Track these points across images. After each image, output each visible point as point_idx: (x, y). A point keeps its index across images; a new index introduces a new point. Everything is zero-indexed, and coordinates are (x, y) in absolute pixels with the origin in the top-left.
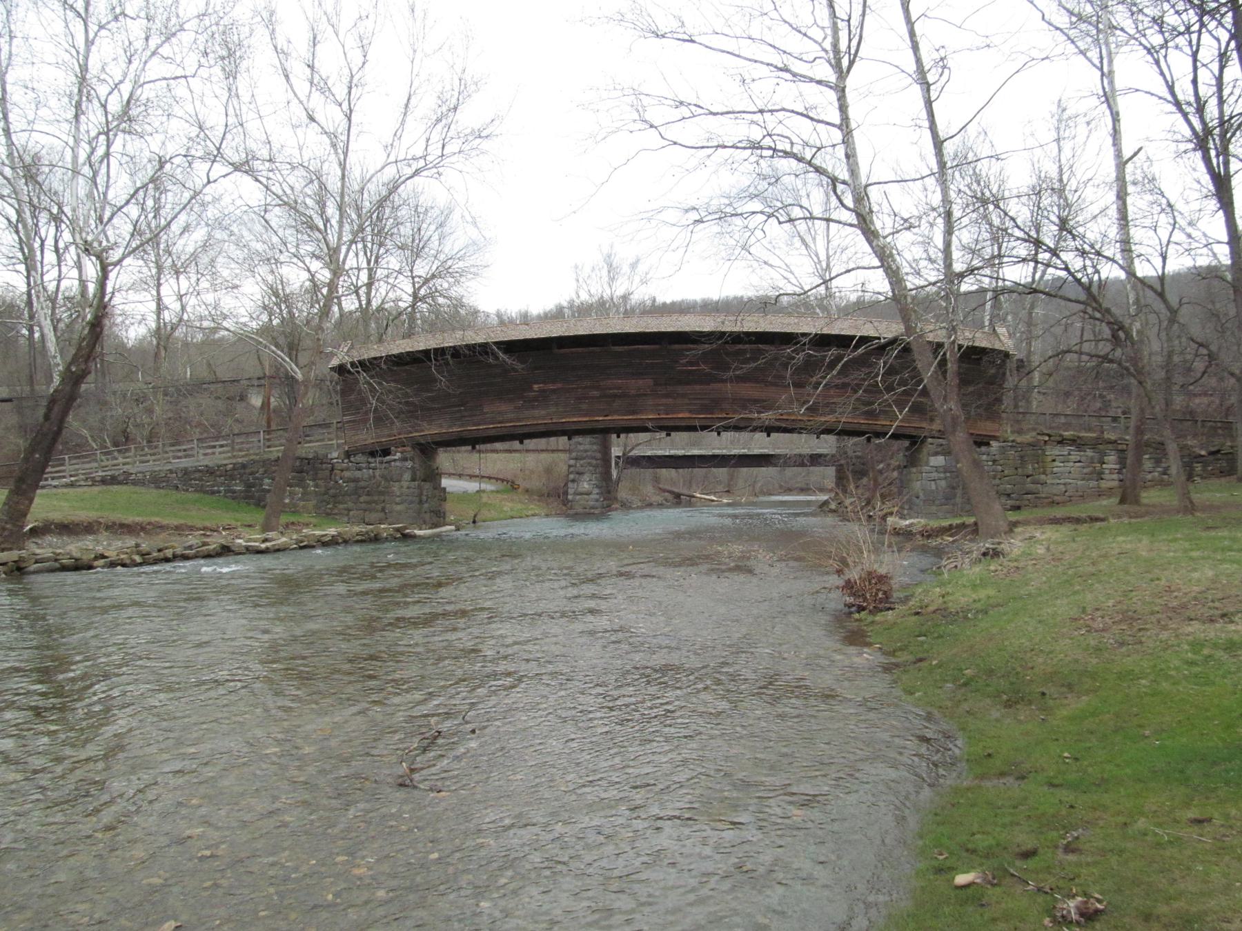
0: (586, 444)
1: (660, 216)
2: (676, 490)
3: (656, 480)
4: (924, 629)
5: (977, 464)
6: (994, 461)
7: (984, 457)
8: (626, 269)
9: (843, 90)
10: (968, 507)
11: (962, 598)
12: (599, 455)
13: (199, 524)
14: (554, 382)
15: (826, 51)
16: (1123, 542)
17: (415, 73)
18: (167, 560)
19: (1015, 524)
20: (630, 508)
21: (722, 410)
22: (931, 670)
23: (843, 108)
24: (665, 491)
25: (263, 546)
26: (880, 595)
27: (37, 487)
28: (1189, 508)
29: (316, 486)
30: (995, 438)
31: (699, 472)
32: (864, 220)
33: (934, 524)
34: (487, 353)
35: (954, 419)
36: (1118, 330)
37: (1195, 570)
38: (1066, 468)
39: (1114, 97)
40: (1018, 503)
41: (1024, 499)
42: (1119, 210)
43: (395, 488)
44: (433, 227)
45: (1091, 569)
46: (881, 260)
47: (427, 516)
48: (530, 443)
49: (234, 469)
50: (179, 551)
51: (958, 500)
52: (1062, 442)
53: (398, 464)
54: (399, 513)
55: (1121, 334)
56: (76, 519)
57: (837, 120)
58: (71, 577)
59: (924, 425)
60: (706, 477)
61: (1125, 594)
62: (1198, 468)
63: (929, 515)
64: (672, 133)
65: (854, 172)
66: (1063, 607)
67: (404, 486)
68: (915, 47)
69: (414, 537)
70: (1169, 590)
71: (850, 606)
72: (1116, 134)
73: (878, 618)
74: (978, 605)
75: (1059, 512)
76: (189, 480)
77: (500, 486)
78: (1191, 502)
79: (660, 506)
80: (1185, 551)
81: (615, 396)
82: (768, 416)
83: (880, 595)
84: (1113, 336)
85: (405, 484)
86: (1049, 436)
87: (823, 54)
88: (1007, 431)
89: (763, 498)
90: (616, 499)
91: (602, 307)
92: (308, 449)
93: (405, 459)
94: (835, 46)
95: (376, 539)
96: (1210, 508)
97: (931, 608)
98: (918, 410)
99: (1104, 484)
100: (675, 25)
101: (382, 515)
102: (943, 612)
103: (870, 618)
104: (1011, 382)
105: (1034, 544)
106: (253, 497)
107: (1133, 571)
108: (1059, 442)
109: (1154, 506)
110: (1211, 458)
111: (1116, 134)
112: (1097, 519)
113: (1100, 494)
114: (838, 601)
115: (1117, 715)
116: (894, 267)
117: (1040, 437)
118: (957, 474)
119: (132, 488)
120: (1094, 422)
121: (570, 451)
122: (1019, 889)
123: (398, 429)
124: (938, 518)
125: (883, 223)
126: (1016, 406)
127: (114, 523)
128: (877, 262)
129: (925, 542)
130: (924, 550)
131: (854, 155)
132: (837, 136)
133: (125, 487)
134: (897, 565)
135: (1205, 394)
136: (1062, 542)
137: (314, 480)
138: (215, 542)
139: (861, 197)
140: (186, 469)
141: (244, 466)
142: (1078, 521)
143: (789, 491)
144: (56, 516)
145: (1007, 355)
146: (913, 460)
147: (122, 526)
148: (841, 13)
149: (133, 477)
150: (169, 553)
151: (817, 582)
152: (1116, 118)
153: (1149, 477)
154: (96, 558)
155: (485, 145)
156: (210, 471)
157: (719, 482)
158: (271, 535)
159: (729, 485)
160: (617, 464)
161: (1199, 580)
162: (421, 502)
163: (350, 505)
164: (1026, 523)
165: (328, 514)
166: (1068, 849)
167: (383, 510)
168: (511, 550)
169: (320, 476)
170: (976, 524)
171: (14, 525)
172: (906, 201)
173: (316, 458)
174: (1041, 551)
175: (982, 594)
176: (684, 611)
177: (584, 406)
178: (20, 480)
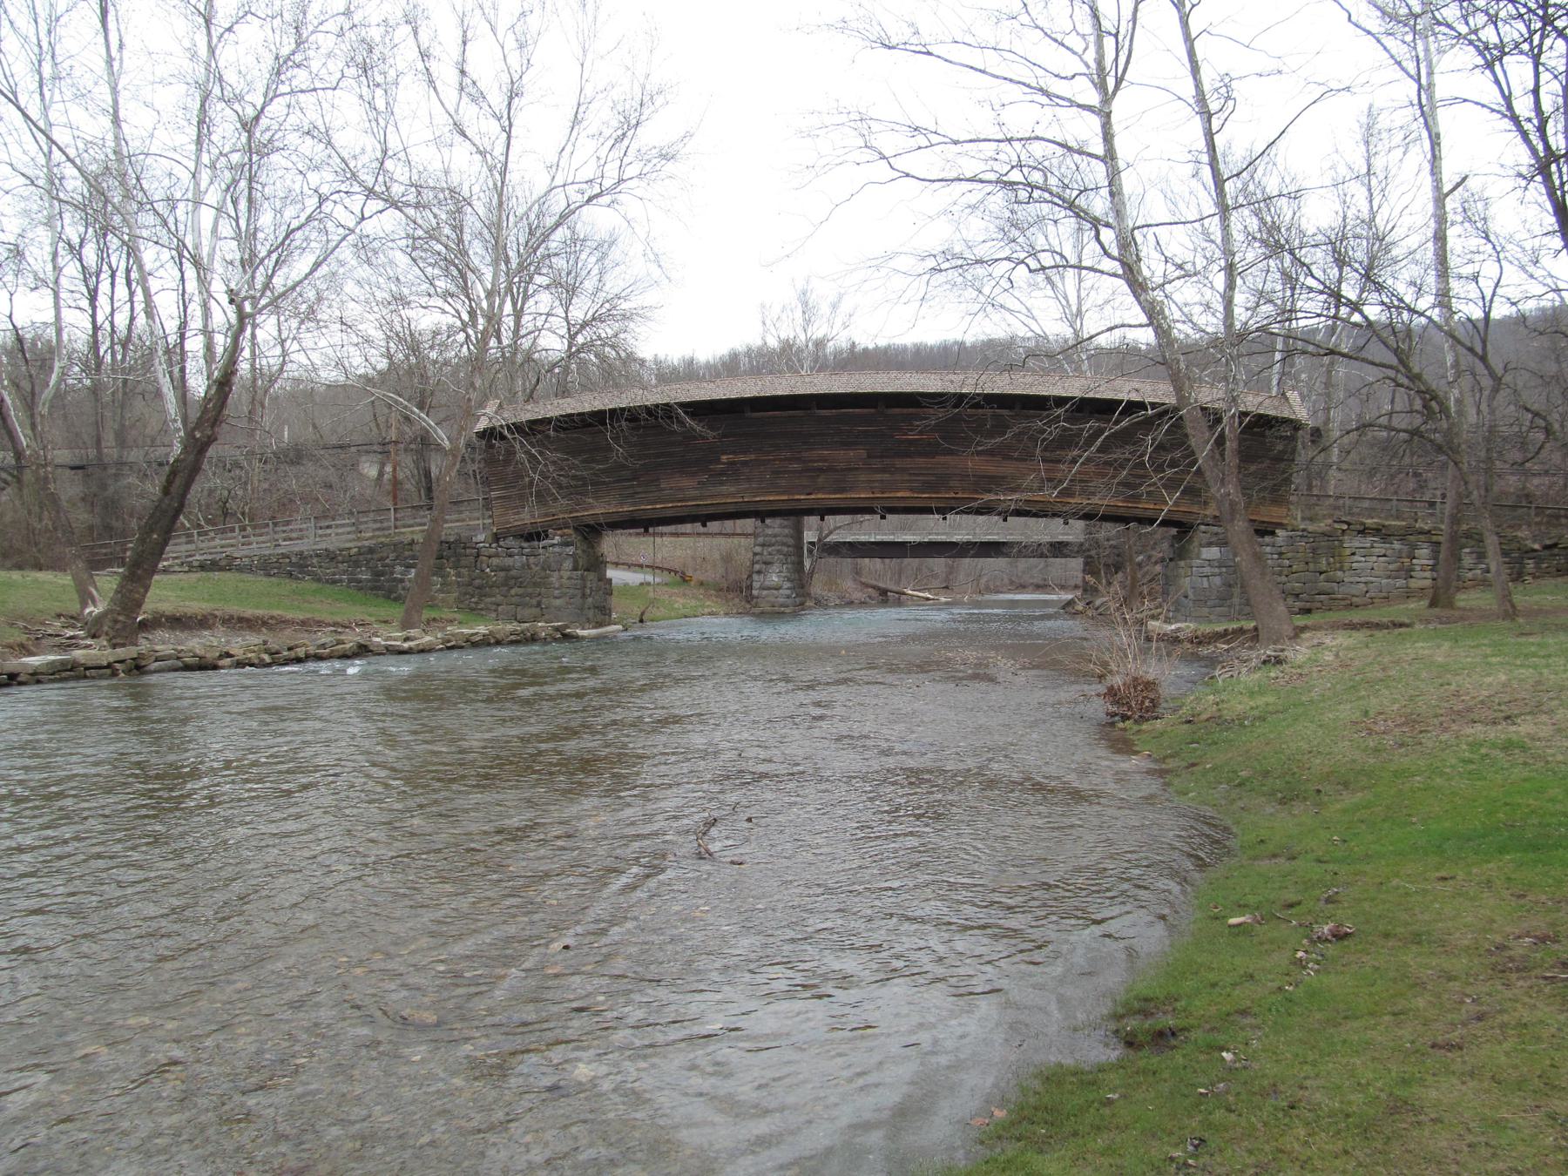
0: (775, 526)
1: (892, 264)
2: (881, 585)
3: (857, 572)
4: (1196, 737)
5: (1258, 558)
6: (1280, 554)
7: (1268, 549)
8: (825, 309)
9: (1108, 115)
10: (1247, 609)
11: (1238, 705)
12: (791, 541)
13: (329, 619)
14: (745, 453)
15: (1088, 67)
16: (1423, 648)
17: (585, 76)
18: (299, 660)
19: (1304, 629)
20: (826, 607)
21: (950, 489)
22: (1205, 772)
23: (1108, 137)
24: (867, 586)
25: (406, 645)
26: (1147, 703)
27: (154, 571)
28: (1511, 613)
29: (458, 575)
30: (1281, 526)
31: (911, 563)
32: (1131, 270)
33: (1207, 629)
34: (670, 418)
35: (1232, 504)
36: (1431, 401)
37: (1489, 675)
38: (1367, 564)
39: (1433, 108)
40: (1308, 605)
41: (1313, 602)
42: (1436, 254)
43: (554, 578)
44: (593, 259)
45: (1380, 675)
46: (1150, 317)
47: (591, 614)
48: (714, 526)
49: (360, 554)
50: (312, 650)
51: (1236, 600)
52: (1364, 531)
53: (557, 549)
54: (558, 609)
55: (1433, 404)
56: (189, 611)
57: (1099, 150)
58: (196, 678)
59: (1195, 509)
60: (919, 569)
61: (1411, 699)
62: (1530, 565)
63: (1198, 619)
64: (901, 163)
65: (1119, 213)
66: (1346, 712)
67: (564, 576)
68: (1195, 69)
69: (577, 638)
70: (1457, 694)
71: (1114, 715)
72: (1435, 159)
73: (1144, 727)
74: (1256, 713)
75: (1356, 616)
76: (295, 568)
77: (667, 577)
78: (1513, 606)
79: (863, 604)
80: (1486, 656)
81: (821, 470)
82: (1012, 499)
83: (1147, 703)
84: (1424, 407)
85: (566, 574)
86: (1349, 524)
87: (1085, 70)
88: (1296, 518)
89: (987, 597)
90: (809, 595)
91: (787, 356)
92: (452, 527)
93: (567, 544)
94: (1100, 62)
95: (533, 639)
96: (1532, 613)
97: (1204, 716)
98: (1192, 492)
99: (1414, 584)
100: (908, 32)
101: (536, 611)
102: (1217, 720)
103: (1136, 728)
104: (1304, 454)
105: (1322, 651)
106: (382, 587)
107: (1424, 675)
108: (1360, 532)
109: (1471, 610)
110: (1547, 552)
111: (1435, 159)
112: (1401, 625)
113: (1409, 595)
114: (1099, 708)
115: (1388, 807)
116: (1165, 326)
117: (1337, 526)
118: (1234, 569)
119: (238, 575)
120: (1405, 507)
121: (755, 535)
122: (1284, 926)
123: (561, 507)
124: (1210, 622)
125: (1152, 267)
126: (1310, 487)
127: (232, 617)
128: (1144, 319)
129: (1196, 649)
130: (1196, 658)
131: (1120, 193)
132: (1099, 171)
133: (228, 575)
134: (1167, 674)
135: (1546, 473)
136: (1353, 649)
137: (455, 568)
138: (351, 639)
139: (1127, 243)
140: (301, 553)
141: (371, 550)
142: (1378, 626)
143: (1022, 587)
144: (167, 608)
145: (1296, 425)
146: (1181, 552)
147: (241, 620)
148: (1107, 25)
149: (238, 562)
150: (301, 652)
151: (1068, 692)
152: (1435, 141)
153: (1470, 575)
154: (221, 657)
155: (670, 167)
156: (331, 556)
157: (935, 576)
158: (413, 632)
159: (947, 579)
160: (810, 552)
161: (1490, 685)
162: (584, 596)
163: (499, 598)
164: (1316, 628)
165: (472, 610)
166: (1328, 901)
167: (539, 604)
168: (704, 655)
169: (463, 562)
170: (1256, 629)
171: (128, 616)
172: (1179, 243)
173: (458, 541)
174: (1329, 657)
175: (1261, 701)
176: (933, 720)
177: (783, 483)
178: (136, 564)
